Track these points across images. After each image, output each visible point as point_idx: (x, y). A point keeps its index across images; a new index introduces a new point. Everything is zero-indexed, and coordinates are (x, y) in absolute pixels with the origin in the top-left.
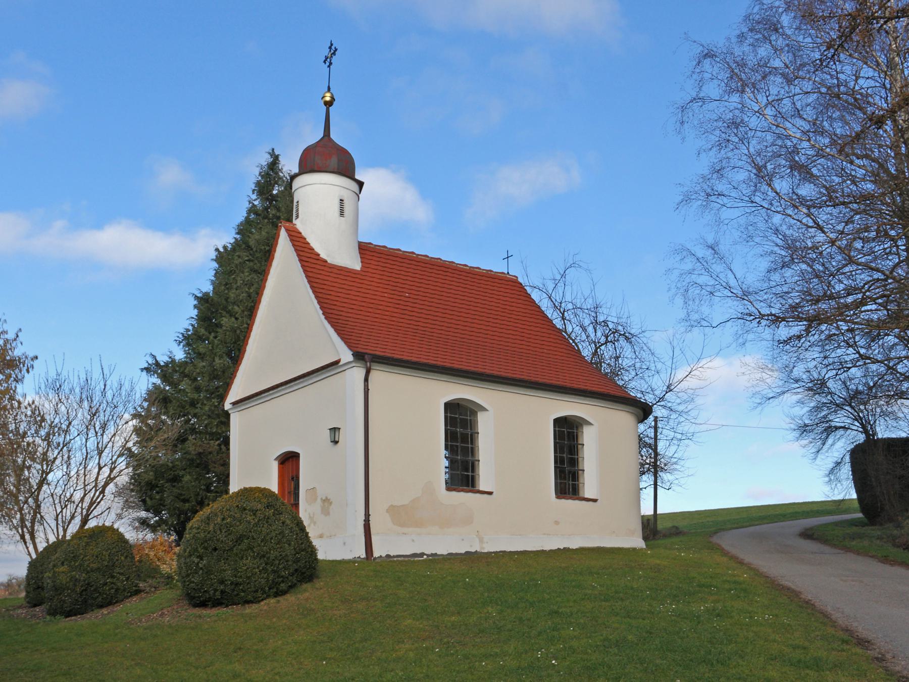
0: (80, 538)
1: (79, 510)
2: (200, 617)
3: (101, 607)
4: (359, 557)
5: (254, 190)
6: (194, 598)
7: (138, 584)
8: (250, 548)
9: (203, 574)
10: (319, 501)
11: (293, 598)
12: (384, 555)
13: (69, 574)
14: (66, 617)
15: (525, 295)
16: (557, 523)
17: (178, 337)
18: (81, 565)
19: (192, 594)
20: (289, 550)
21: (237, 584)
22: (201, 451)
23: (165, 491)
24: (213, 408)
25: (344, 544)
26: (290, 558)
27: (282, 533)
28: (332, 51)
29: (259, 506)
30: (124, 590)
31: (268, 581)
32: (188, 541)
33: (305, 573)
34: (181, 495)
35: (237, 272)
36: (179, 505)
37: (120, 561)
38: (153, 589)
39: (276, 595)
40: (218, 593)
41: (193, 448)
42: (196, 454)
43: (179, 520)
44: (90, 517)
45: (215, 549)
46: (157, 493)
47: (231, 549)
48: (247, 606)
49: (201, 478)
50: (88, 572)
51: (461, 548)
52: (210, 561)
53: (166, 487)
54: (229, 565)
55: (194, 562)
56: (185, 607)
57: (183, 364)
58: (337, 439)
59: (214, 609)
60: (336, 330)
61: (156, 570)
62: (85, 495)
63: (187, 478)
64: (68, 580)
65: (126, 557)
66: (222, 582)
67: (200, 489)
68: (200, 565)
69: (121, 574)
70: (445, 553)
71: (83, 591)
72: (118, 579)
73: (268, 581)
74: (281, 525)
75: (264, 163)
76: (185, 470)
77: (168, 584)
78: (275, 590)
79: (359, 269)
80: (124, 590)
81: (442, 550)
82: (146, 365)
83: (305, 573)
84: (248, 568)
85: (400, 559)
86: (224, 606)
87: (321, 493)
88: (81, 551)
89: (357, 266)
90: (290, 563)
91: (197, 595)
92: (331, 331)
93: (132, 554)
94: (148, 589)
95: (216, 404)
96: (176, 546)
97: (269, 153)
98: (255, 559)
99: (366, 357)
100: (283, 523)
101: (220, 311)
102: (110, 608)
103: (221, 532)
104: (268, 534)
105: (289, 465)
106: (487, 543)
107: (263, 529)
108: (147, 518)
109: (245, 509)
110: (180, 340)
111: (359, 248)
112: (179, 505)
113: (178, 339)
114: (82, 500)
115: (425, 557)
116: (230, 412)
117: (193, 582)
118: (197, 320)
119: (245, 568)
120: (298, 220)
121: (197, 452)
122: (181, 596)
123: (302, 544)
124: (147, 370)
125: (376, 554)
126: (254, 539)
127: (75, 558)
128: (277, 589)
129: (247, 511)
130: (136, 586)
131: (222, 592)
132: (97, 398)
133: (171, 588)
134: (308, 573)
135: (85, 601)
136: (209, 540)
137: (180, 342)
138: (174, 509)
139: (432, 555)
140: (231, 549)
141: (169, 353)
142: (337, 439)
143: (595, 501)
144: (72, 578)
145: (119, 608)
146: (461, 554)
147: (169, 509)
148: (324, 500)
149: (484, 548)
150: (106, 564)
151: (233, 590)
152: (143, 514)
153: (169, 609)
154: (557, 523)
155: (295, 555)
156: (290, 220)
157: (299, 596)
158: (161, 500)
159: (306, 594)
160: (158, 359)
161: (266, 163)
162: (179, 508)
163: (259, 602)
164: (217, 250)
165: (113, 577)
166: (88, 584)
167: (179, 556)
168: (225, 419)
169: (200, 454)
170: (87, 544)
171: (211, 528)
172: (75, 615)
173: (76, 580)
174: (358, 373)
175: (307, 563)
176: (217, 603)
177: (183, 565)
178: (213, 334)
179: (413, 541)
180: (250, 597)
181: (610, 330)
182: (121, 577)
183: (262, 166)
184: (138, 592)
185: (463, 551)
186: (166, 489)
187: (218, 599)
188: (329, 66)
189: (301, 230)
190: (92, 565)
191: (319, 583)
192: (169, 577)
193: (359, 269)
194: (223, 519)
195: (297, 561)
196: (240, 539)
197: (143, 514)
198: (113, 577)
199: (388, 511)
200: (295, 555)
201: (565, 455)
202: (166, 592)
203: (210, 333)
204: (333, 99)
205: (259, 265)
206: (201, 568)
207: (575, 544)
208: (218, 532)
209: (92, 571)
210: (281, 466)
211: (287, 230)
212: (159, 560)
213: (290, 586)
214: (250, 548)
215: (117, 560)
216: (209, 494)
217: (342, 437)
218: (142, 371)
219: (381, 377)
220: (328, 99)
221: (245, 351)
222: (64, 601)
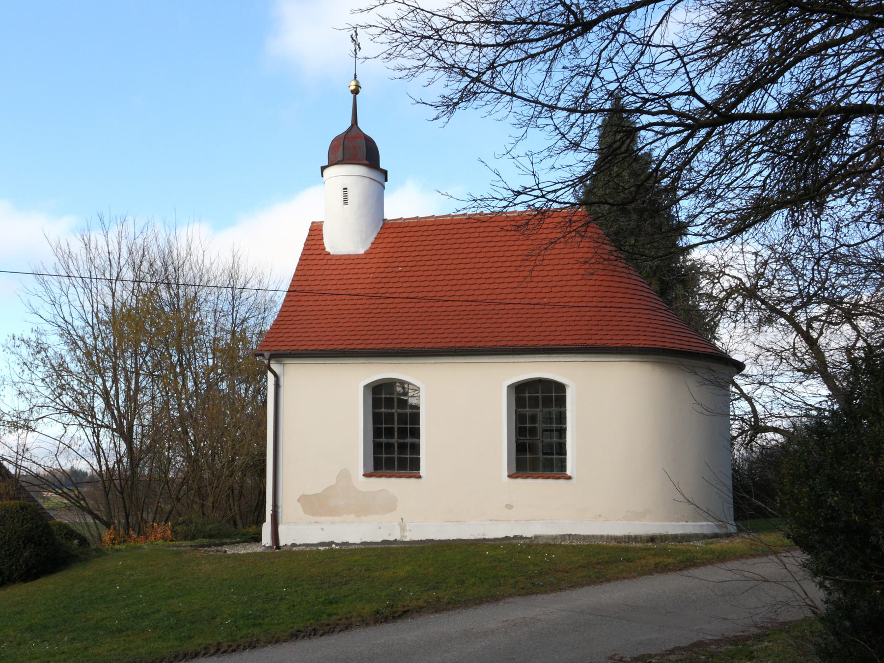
12: (289, 544)
16: (509, 507)
51: (377, 536)
154: (509, 507)
179: (322, 529)
185: (379, 540)
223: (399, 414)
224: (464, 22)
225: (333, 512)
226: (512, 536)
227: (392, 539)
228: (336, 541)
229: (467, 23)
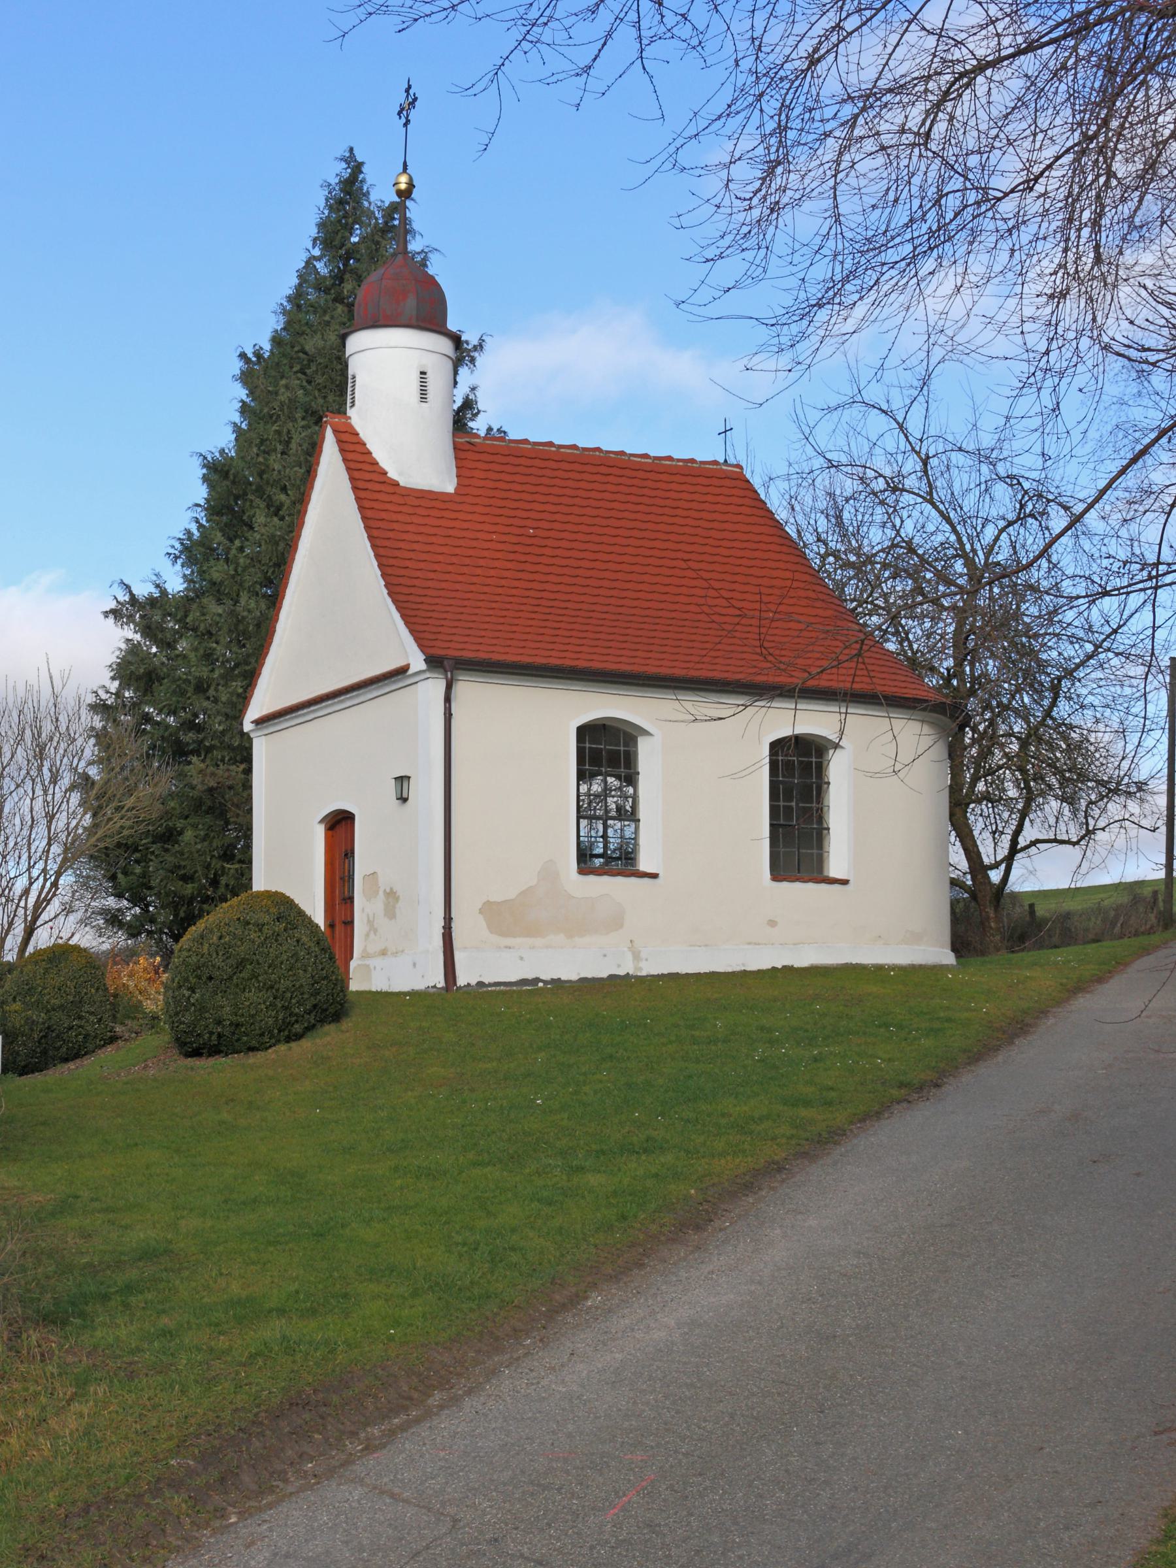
0: (36, 963)
1: (21, 912)
2: (192, 1069)
3: (66, 1060)
4: (434, 987)
5: (315, 240)
6: (185, 1044)
7: (113, 1027)
8: (255, 976)
9: (195, 1011)
10: (381, 893)
11: (309, 1044)
12: (473, 983)
13: (23, 1015)
14: (21, 1075)
15: (753, 503)
16: (772, 923)
17: (173, 547)
18: (38, 1002)
19: (182, 1039)
20: (304, 979)
21: (238, 1025)
22: (212, 784)
23: (152, 860)
24: (234, 699)
25: (414, 965)
26: (306, 989)
27: (295, 954)
28: (410, 100)
29: (266, 918)
30: (95, 1037)
31: (277, 1020)
32: (177, 967)
33: (326, 1010)
34: (179, 867)
35: (282, 418)
36: (175, 886)
37: (89, 995)
38: (133, 1035)
39: (288, 1040)
40: (214, 1037)
41: (200, 780)
42: (205, 791)
43: (176, 916)
44: (38, 923)
45: (210, 978)
46: (138, 862)
47: (230, 978)
48: (251, 1054)
49: (212, 834)
50: (48, 1011)
51: (601, 970)
52: (204, 994)
53: (153, 853)
54: (227, 999)
55: (184, 995)
56: (175, 1057)
57: (186, 602)
58: (405, 795)
59: (210, 1059)
60: (403, 616)
61: (138, 1006)
62: (31, 884)
63: (189, 835)
64: (22, 1022)
65: (97, 989)
66: (219, 1022)
67: (213, 856)
68: (192, 1000)
69: (92, 1013)
70: (574, 977)
71: (41, 1038)
72: (88, 1021)
73: (277, 1020)
74: (295, 944)
75: (334, 181)
76: (187, 817)
77: (153, 1027)
78: (286, 1033)
79: (452, 491)
80: (95, 1037)
81: (569, 972)
82: (113, 605)
83: (326, 1010)
84: (251, 1004)
85: (498, 988)
86: (222, 1055)
87: (384, 883)
88: (38, 982)
89: (446, 483)
90: (306, 996)
91: (188, 1040)
92: (396, 616)
93: (105, 985)
94: (127, 1035)
95: (240, 690)
96: (164, 972)
97: (343, 159)
98: (260, 991)
99: (445, 662)
100: (298, 941)
101: (250, 497)
102: (78, 1061)
103: (218, 954)
104: (277, 957)
105: (341, 830)
106: (647, 960)
107: (271, 950)
108: (119, 910)
109: (248, 923)
110: (177, 552)
111: (455, 448)
112: (175, 886)
113: (172, 551)
114: (26, 892)
115: (541, 984)
116: (252, 735)
117: (184, 1023)
118: (206, 509)
119: (248, 1003)
120: (353, 409)
121: (206, 787)
122: (169, 1043)
123: (322, 970)
124: (116, 613)
125: (461, 981)
126: (259, 964)
127: (30, 991)
128: (290, 1031)
129: (251, 926)
130: (111, 1031)
131: (220, 1036)
132: (48, 727)
133: (157, 1033)
134: (330, 1010)
135: (45, 1052)
136: (203, 966)
137: (176, 558)
138: (167, 895)
139: (553, 981)
140: (230, 978)
141: (154, 578)
142: (405, 795)
143: (845, 882)
144: (28, 1019)
145: (88, 1061)
146: (602, 979)
147: (158, 895)
148: (388, 894)
149: (641, 969)
150: (72, 999)
151: (234, 1033)
152: (111, 902)
153: (155, 1060)
154: (772, 923)
155: (313, 985)
156: (341, 410)
157: (318, 1041)
158: (144, 875)
159: (328, 1038)
160: (134, 592)
161: (337, 181)
162: (175, 893)
163: (267, 1049)
164: (243, 356)
165: (80, 1018)
166: (49, 1028)
167: (166, 987)
168: (243, 755)
169: (211, 790)
170: (46, 971)
171: (205, 951)
172: (33, 1072)
173: (34, 1021)
174: (434, 687)
175: (330, 997)
176: (215, 1051)
177: (170, 1000)
178: (237, 543)
179: (521, 958)
180: (254, 1043)
181: (1026, 492)
182: (92, 1018)
183: (330, 185)
184: (113, 1039)
185: (605, 975)
186: (153, 857)
187: (214, 1045)
188: (406, 125)
189: (358, 429)
190: (53, 1001)
191: (346, 1024)
192: (155, 1018)
193: (452, 491)
194: (220, 938)
195: (317, 993)
196: (241, 964)
197: (111, 902)
198: (80, 1018)
199: (481, 911)
200: (313, 985)
201: (793, 804)
202: (150, 1038)
203: (231, 540)
204: (411, 185)
205: (321, 401)
206: (193, 1004)
207: (803, 959)
208: (214, 955)
209: (54, 1010)
210: (330, 832)
211: (335, 431)
212: (140, 993)
213: (306, 1028)
214: (255, 976)
215: (86, 994)
216: (229, 866)
217: (415, 790)
218: (107, 617)
219: (470, 689)
220: (403, 186)
221: (275, 631)
222: (18, 1053)
223: (609, 751)
224: (884, 66)
225: (532, 931)
226: (780, 967)
227: (622, 972)
228: (542, 978)
229: (887, 63)
